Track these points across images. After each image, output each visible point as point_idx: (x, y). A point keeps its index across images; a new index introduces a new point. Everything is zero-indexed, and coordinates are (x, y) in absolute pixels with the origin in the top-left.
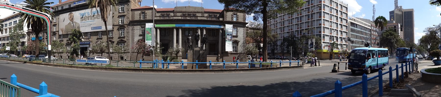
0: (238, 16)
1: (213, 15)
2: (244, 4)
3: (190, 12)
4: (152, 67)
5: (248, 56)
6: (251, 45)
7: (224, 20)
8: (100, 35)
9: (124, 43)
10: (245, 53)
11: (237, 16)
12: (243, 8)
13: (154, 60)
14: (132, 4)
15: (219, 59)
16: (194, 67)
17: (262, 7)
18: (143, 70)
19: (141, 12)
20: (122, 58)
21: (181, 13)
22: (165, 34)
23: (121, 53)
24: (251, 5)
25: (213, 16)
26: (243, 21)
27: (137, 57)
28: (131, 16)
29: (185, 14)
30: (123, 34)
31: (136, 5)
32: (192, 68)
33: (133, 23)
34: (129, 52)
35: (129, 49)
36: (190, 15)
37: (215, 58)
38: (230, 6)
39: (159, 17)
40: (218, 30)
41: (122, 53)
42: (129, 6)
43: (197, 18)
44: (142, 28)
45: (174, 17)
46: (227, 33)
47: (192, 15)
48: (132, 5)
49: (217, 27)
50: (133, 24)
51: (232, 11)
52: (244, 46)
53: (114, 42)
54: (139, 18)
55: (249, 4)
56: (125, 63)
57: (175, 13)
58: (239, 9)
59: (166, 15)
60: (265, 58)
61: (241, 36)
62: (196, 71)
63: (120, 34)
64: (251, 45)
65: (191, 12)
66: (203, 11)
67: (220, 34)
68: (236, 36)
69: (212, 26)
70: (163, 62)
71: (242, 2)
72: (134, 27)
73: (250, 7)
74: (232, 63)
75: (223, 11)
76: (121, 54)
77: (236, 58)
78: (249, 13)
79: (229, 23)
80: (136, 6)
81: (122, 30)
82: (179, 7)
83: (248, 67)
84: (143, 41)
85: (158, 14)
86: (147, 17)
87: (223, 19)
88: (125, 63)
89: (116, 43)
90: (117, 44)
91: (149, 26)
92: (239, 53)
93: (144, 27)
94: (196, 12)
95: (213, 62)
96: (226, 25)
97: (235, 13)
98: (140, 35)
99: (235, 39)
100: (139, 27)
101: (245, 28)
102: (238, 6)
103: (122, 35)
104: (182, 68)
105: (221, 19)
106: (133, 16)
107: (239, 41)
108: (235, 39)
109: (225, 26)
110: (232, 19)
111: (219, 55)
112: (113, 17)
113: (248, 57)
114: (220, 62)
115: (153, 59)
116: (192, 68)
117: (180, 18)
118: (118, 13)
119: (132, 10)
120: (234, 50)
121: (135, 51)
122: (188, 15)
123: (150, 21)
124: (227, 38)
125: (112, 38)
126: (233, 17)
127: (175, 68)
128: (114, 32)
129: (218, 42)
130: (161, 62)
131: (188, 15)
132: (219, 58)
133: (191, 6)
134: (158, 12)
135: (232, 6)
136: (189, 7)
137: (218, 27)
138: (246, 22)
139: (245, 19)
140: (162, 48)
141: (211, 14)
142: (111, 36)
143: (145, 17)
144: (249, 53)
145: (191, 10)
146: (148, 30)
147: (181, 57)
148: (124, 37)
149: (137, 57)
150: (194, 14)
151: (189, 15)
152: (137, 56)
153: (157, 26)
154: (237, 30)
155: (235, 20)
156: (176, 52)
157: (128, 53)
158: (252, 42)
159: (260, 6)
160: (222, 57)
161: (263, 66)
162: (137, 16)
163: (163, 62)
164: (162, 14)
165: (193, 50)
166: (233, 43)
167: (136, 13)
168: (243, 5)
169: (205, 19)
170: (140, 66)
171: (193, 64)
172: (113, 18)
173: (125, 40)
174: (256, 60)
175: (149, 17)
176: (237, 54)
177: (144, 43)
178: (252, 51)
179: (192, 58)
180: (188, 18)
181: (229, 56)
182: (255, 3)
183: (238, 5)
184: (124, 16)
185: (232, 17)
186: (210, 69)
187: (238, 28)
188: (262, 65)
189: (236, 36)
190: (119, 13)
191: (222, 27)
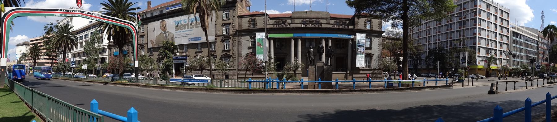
0: (372, 23)
2: (380, 8)
3: (312, 18)
4: (264, 87)
5: (385, 72)
6: (388, 59)
9: (229, 57)
11: (371, 23)
12: (378, 13)
13: (266, 78)
14: (238, 9)
15: (348, 77)
17: (402, 12)
19: (250, 19)
20: (227, 77)
21: (300, 20)
25: (341, 23)
27: (245, 75)
29: (306, 21)
30: (227, 46)
31: (244, 10)
33: (240, 33)
36: (312, 22)
37: (342, 75)
39: (273, 24)
40: (347, 40)
42: (234, 12)
43: (321, 26)
44: (252, 38)
46: (359, 45)
47: (314, 22)
48: (239, 11)
49: (346, 36)
50: (239, 33)
51: (365, 16)
53: (216, 57)
54: (248, 26)
57: (292, 20)
60: (405, 75)
64: (388, 59)
65: (314, 19)
66: (329, 16)
67: (350, 46)
70: (278, 81)
72: (242, 37)
74: (364, 82)
75: (353, 17)
76: (226, 72)
79: (361, 31)
80: (244, 12)
81: (226, 42)
82: (298, 12)
86: (258, 24)
87: (354, 27)
88: (231, 83)
89: (219, 57)
91: (260, 36)
92: (373, 69)
93: (255, 38)
94: (320, 18)
96: (357, 34)
97: (369, 19)
98: (249, 48)
99: (369, 51)
100: (248, 37)
101: (381, 38)
102: (372, 10)
105: (351, 27)
106: (240, 24)
108: (369, 51)
109: (355, 35)
110: (364, 27)
111: (348, 72)
112: (216, 25)
113: (384, 73)
117: (299, 26)
119: (239, 17)
121: (243, 68)
122: (309, 21)
123: (262, 30)
124: (359, 50)
125: (215, 51)
126: (365, 25)
127: (292, 87)
128: (216, 44)
129: (347, 56)
132: (348, 75)
134: (272, 19)
135: (365, 10)
136: (311, 11)
138: (383, 30)
141: (338, 21)
142: (213, 49)
145: (313, 15)
146: (259, 42)
147: (301, 74)
148: (229, 51)
149: (245, 75)
150: (318, 20)
151: (311, 22)
152: (246, 73)
153: (270, 36)
154: (371, 40)
155: (368, 27)
156: (295, 67)
158: (389, 55)
159: (400, 10)
160: (351, 74)
161: (402, 85)
162: (245, 24)
163: (278, 81)
164: (276, 21)
165: (315, 66)
166: (366, 56)
167: (244, 20)
168: (379, 9)
169: (331, 26)
173: (231, 53)
175: (260, 26)
176: (371, 70)
179: (314, 76)
182: (393, 7)
183: (372, 9)
184: (229, 24)
185: (364, 24)
187: (373, 38)
188: (338, 85)
189: (370, 49)
190: (223, 20)
191: (352, 37)
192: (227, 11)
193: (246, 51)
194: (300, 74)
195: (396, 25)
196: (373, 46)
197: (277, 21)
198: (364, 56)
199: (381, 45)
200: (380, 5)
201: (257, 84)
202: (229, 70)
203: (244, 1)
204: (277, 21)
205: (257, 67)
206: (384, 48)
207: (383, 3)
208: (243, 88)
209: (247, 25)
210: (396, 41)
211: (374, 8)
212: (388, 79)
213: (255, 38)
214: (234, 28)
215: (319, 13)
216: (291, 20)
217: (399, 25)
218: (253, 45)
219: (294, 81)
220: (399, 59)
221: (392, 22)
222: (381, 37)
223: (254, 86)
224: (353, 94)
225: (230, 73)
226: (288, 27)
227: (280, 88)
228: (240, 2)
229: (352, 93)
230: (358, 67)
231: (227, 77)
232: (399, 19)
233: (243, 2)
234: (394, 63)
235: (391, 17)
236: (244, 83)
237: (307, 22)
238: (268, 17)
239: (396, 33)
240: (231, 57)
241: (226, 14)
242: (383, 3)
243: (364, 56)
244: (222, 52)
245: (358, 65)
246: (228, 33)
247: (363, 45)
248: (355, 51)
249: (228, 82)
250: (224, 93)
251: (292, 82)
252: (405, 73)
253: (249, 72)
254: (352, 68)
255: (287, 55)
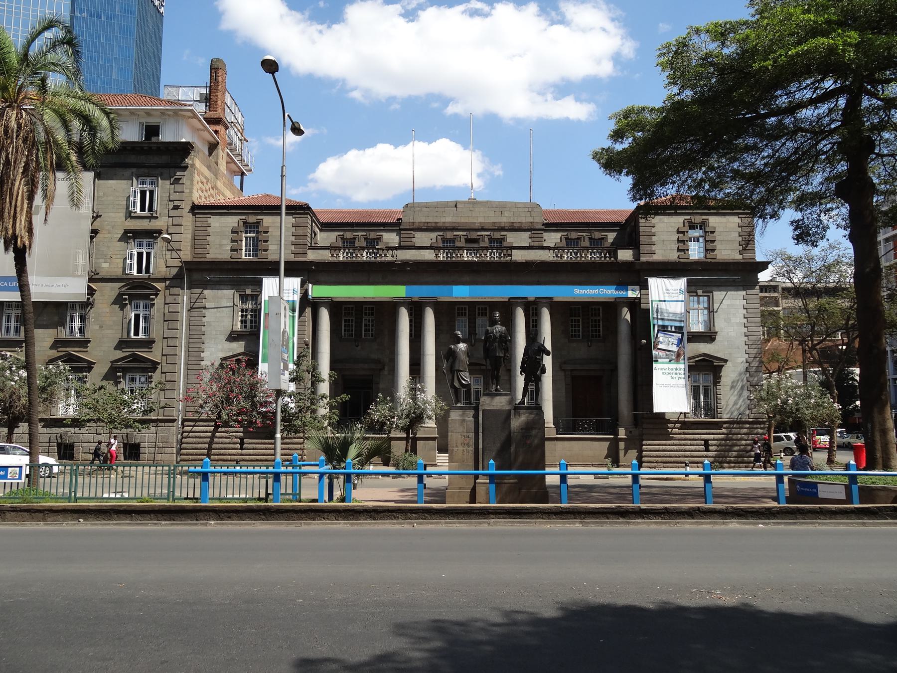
0: (713, 232)
1: (587, 239)
2: (736, 165)
3: (477, 226)
4: (263, 495)
5: (782, 435)
6: (794, 378)
7: (642, 260)
8: (13, 324)
9: (144, 370)
10: (763, 423)
11: (706, 232)
12: (731, 189)
13: (279, 458)
14: (197, 178)
15: (622, 453)
16: (481, 492)
17: (843, 167)
18: (214, 515)
19: (241, 223)
20: (132, 451)
21: (434, 235)
22: (359, 334)
23: (127, 427)
24: (774, 166)
25: (587, 244)
26: (738, 257)
27: (211, 443)
28: (189, 236)
29: (454, 238)
30: (142, 324)
31: (220, 184)
32: (473, 500)
34: (173, 421)
35: (173, 403)
36: (476, 240)
37: (599, 447)
38: (663, 185)
39: (332, 248)
40: (611, 308)
41: (131, 427)
42: (178, 188)
43: (511, 255)
44: (244, 298)
45: (399, 252)
46: (660, 323)
47: (486, 243)
48: (196, 187)
49: (607, 292)
50: (196, 276)
51: (671, 208)
52: (753, 386)
53: (89, 367)
54: (232, 250)
55: (766, 161)
56: (146, 477)
57: (404, 234)
58: (713, 194)
59: (363, 239)
60: (879, 446)
61: (733, 334)
62: (484, 513)
63: (125, 325)
64: (794, 378)
65: (483, 229)
66: (538, 220)
67: (624, 331)
68: (709, 336)
69: (582, 292)
70: (327, 468)
71: (724, 156)
72: (206, 292)
73: (769, 176)
74: (687, 475)
75: (634, 217)
76: (129, 430)
77: (711, 448)
78: (769, 210)
79: (667, 270)
80: (220, 193)
81: (137, 307)
82: (427, 205)
83: (776, 499)
84: (243, 365)
85: (325, 235)
86: (272, 246)
87: (637, 256)
88: (146, 477)
89: (101, 369)
90: (106, 377)
92: (725, 422)
93: (256, 297)
95: (593, 465)
96: (653, 282)
97: (698, 219)
98: (233, 337)
99: (704, 348)
100: (229, 293)
101: (756, 293)
102: (702, 180)
103: (137, 333)
104: (416, 499)
105: (625, 255)
106: (199, 238)
107: (726, 361)
108: (704, 348)
109: (644, 286)
110: (679, 250)
111: (622, 434)
112: (95, 232)
113: (779, 439)
114: (625, 466)
115: (274, 455)
116: (473, 500)
117: (429, 255)
118: (122, 215)
119: (196, 209)
120: (697, 407)
121: (204, 417)
122: (468, 240)
125: (84, 343)
126: (683, 242)
127: (396, 496)
128: (92, 314)
129: (614, 370)
130: (316, 469)
131: (468, 240)
132: (622, 445)
133: (479, 199)
134: (327, 226)
135: (674, 183)
137: (609, 292)
138: (760, 258)
139: (748, 242)
140: (338, 399)
141: (574, 235)
142: (78, 335)
143: (262, 245)
144: (783, 421)
147: (435, 444)
148: (148, 344)
149: (211, 443)
150: (497, 235)
151: (473, 244)
152: (213, 437)
153: (316, 291)
154: (710, 301)
155: (695, 252)
156: (407, 416)
157: (167, 424)
158: (800, 359)
159: (830, 161)
160: (636, 443)
161: (868, 494)
163: (327, 468)
164: (342, 238)
165: (476, 409)
166: (691, 369)
167: (217, 225)
168: (733, 170)
170: (203, 491)
171: (476, 477)
172: (92, 238)
173: (154, 355)
174: (830, 461)
176: (717, 425)
177: (248, 372)
178: (798, 410)
179: (472, 449)
180: (467, 257)
181: (672, 439)
182: (795, 153)
183: (704, 173)
184: (152, 235)
185: (679, 241)
186: (562, 505)
187: (718, 295)
188: (861, 489)
189: (709, 336)
190: (130, 215)
191: (632, 293)
192: (148, 180)
193: (220, 347)
194: (431, 442)
195: (818, 227)
196: (720, 325)
197: (349, 235)
198: (682, 366)
199: (759, 320)
200: (733, 153)
201: (257, 481)
202: (143, 422)
203: (220, 151)
204: (349, 235)
205: (259, 413)
206: (772, 332)
207: (751, 141)
208: (76, 499)
209: (229, 246)
210: (824, 300)
211: (711, 168)
212: (793, 466)
213: (256, 299)
214: (174, 255)
215: (501, 207)
216: (399, 234)
217: (833, 227)
218: (248, 324)
219: (404, 469)
220: (847, 376)
221: (798, 215)
222: (753, 288)
223: (243, 491)
224: (631, 527)
225: (146, 437)
226: (386, 259)
227: (335, 498)
228: (207, 152)
229: (629, 523)
230: (664, 414)
231: (132, 451)
232: (832, 200)
233: (218, 155)
234: (823, 395)
235: (791, 197)
236: (80, 479)
237: (458, 244)
238: (312, 221)
239: (820, 263)
240: (154, 369)
241: (143, 193)
242: (751, 141)
243: (681, 366)
244: (116, 348)
245: (659, 407)
246: (148, 271)
247: (678, 324)
248: (648, 349)
249: (133, 473)
250: (83, 525)
251: (396, 475)
252: (878, 437)
253: (224, 435)
254: (635, 417)
255: (382, 369)
